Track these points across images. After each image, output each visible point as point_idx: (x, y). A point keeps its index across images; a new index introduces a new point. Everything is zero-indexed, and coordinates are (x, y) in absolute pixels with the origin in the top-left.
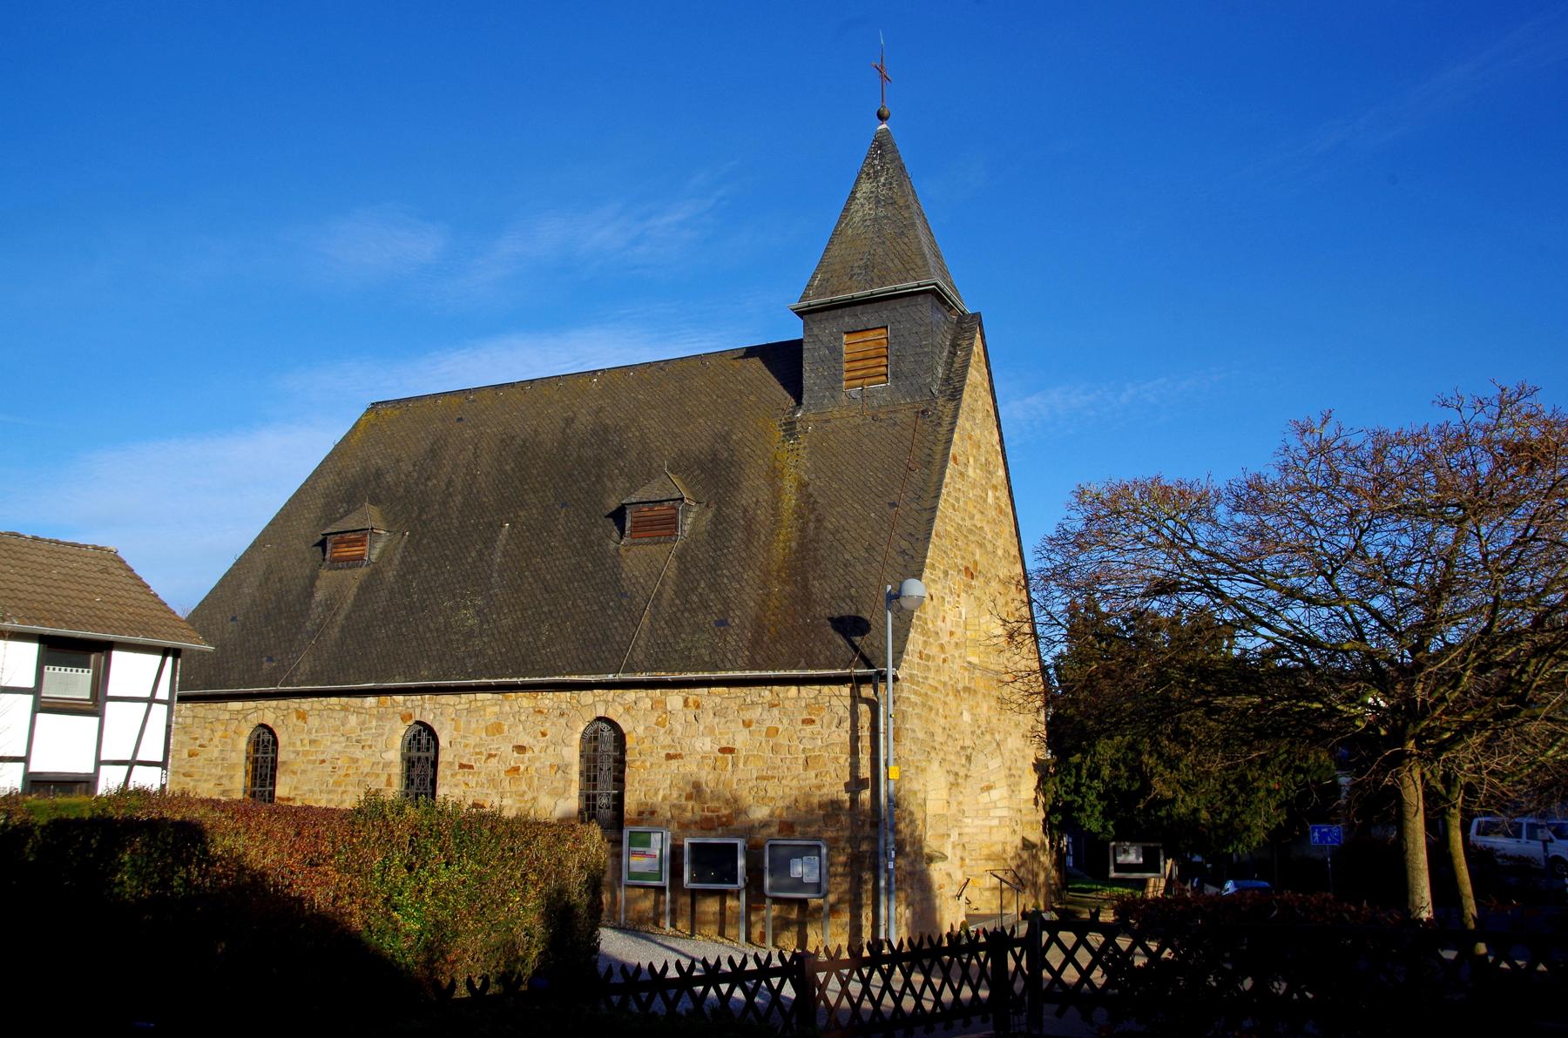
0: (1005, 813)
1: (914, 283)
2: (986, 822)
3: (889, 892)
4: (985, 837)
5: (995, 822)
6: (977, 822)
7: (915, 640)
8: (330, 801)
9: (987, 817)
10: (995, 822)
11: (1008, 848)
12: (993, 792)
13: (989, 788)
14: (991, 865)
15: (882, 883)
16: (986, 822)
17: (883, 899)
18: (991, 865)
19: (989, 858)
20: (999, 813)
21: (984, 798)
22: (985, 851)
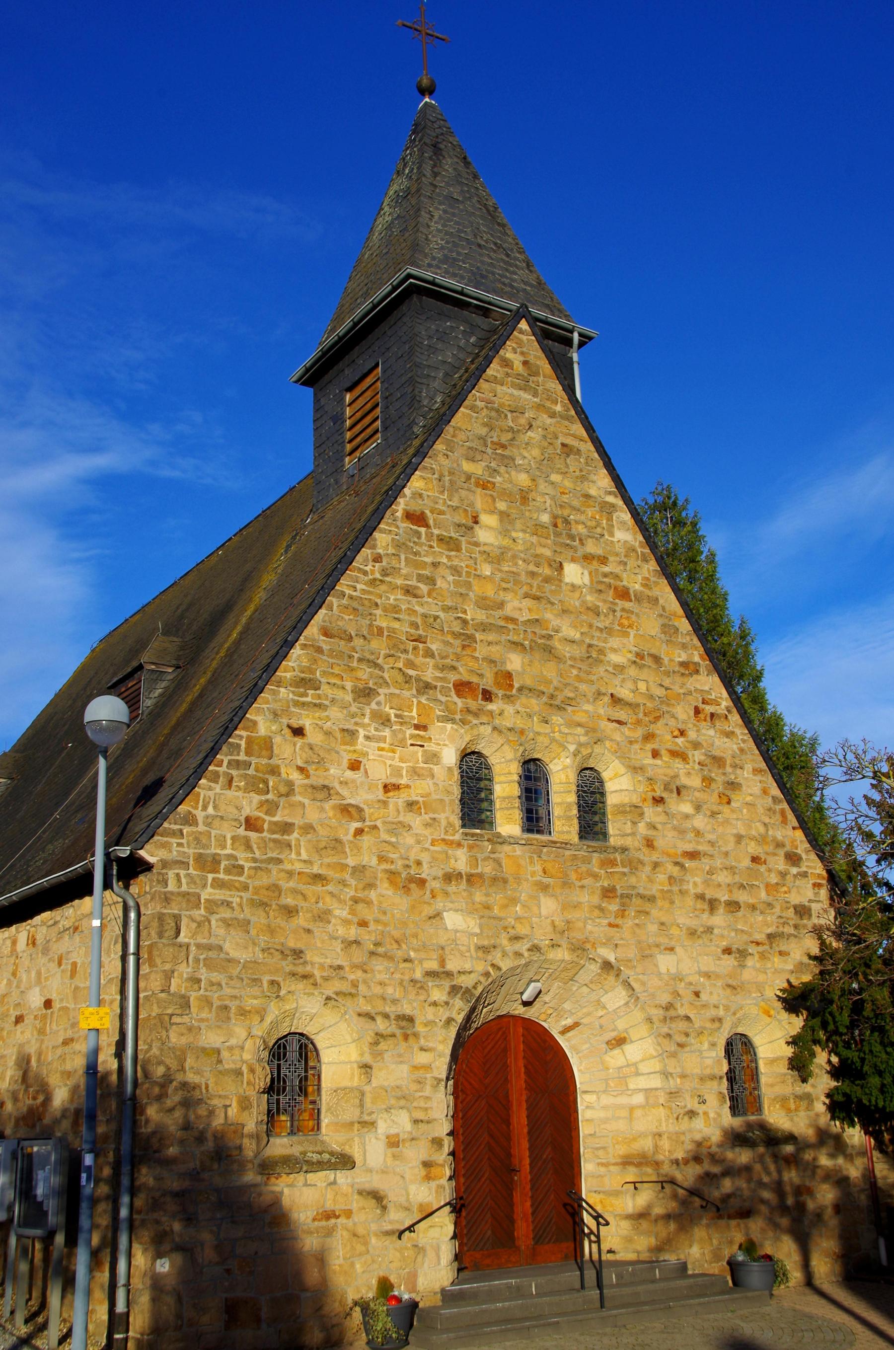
0: (656, 1082)
1: (387, 288)
2: (623, 1100)
3: (131, 1229)
4: (621, 1125)
5: (639, 1099)
6: (606, 1100)
7: (217, 805)
8: (807, 852)
9: (625, 1091)
10: (639, 1099)
11: (665, 1144)
12: (627, 1048)
13: (620, 1042)
14: (631, 1174)
15: (124, 1213)
16: (623, 1100)
17: (123, 1240)
18: (631, 1174)
19: (626, 1162)
20: (643, 1083)
21: (616, 1059)
22: (622, 1150)
